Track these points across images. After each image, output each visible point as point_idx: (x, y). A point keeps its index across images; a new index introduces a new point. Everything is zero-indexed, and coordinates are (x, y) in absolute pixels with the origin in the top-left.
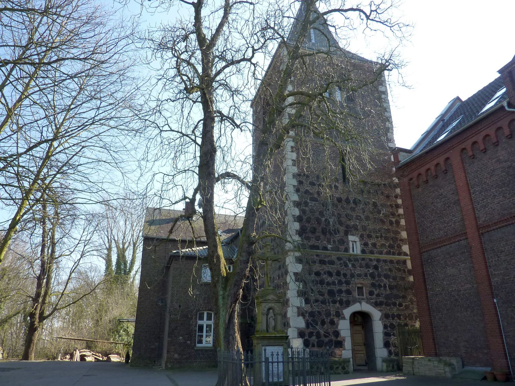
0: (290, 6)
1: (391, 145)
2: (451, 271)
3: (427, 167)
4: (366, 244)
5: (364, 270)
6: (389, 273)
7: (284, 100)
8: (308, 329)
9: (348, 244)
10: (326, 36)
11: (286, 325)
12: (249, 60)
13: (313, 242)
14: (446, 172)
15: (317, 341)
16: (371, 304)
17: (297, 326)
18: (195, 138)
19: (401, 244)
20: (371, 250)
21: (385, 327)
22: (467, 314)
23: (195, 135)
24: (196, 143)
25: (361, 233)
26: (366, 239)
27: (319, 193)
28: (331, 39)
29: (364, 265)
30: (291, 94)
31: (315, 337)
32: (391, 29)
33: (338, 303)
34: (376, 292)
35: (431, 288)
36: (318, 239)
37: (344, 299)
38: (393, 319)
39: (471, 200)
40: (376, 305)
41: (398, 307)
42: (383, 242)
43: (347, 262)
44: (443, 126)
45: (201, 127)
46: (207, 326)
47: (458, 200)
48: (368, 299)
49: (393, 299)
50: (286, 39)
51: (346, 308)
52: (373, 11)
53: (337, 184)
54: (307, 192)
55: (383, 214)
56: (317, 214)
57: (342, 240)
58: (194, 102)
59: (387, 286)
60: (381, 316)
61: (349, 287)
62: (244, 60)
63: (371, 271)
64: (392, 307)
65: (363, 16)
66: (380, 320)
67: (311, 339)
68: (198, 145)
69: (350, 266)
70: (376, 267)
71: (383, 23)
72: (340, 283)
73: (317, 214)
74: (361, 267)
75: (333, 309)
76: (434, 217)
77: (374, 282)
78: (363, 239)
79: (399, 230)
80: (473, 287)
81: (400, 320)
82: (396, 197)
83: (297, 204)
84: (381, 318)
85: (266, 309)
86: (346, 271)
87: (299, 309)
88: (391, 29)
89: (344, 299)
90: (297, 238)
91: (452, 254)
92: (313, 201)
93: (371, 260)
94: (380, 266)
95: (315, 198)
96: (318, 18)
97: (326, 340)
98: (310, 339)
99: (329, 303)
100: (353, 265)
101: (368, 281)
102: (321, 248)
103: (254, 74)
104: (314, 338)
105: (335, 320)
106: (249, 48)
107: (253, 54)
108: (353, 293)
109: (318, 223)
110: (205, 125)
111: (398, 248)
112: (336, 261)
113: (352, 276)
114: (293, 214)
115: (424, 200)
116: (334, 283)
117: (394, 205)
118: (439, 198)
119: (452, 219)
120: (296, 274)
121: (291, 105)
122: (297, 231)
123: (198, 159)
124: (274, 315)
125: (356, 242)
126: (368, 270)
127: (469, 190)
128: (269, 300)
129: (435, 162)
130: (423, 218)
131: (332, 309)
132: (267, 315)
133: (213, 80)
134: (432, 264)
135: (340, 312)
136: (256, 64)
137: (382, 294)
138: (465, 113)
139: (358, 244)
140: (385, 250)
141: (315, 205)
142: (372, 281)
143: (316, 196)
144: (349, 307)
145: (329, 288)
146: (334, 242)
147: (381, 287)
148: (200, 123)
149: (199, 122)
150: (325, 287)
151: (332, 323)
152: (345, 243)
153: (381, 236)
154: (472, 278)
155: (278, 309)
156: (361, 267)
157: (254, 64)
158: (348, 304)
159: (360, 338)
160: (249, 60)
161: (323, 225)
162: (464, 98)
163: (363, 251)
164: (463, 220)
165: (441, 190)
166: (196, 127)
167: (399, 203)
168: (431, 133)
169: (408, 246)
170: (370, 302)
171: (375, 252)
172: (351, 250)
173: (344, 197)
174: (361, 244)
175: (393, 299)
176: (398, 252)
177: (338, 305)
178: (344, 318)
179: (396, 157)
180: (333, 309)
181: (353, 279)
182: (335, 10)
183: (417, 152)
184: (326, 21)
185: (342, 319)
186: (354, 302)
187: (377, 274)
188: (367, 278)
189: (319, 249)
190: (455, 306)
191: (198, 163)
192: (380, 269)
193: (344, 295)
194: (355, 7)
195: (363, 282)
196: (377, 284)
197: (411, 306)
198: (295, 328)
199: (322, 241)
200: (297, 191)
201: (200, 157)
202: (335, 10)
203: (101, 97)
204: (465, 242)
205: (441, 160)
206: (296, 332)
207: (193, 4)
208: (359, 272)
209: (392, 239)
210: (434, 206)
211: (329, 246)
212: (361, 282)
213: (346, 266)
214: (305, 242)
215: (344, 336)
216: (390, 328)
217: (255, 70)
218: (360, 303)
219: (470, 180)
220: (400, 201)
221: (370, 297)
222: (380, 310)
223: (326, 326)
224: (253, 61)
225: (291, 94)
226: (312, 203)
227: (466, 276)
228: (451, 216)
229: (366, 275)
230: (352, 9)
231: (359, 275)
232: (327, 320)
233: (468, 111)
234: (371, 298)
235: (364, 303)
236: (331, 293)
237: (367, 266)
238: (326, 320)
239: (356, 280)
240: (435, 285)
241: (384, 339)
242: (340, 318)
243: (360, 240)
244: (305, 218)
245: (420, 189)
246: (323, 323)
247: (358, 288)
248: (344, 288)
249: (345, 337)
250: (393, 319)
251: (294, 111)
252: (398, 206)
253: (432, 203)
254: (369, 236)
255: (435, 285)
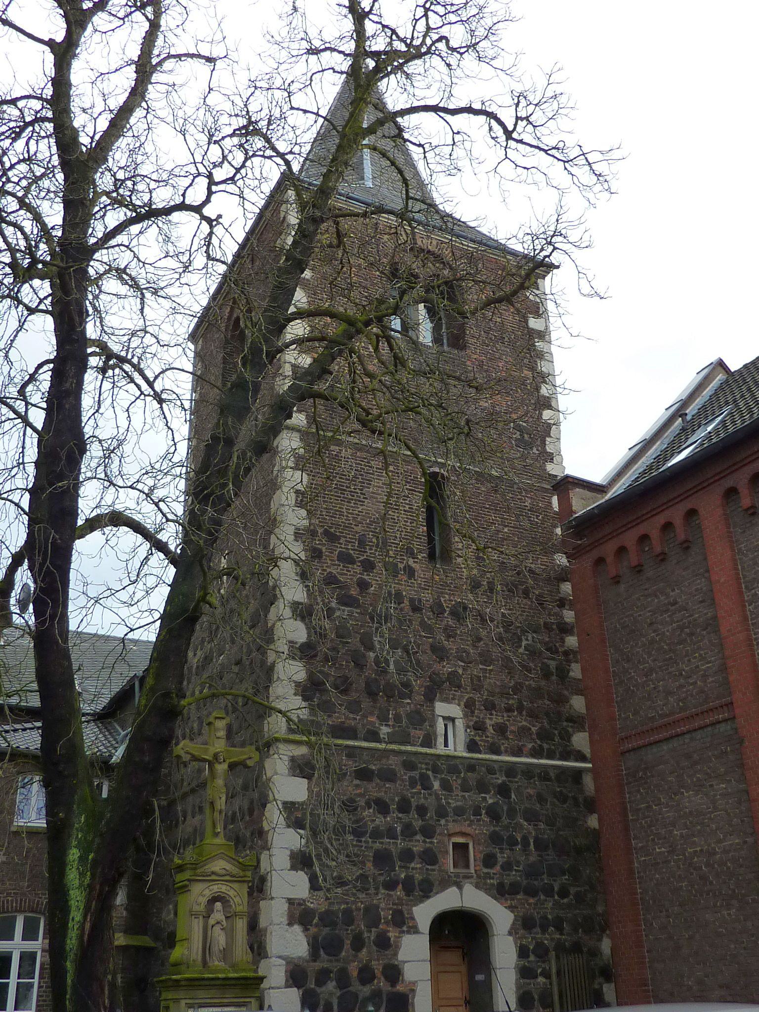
0: (311, 80)
1: (551, 468)
2: (692, 800)
3: (642, 529)
4: (479, 727)
5: (474, 798)
6: (538, 807)
7: (281, 328)
8: (315, 961)
9: (433, 725)
10: (400, 172)
11: (258, 949)
12: (197, 209)
13: (341, 716)
14: (686, 546)
15: (338, 994)
16: (488, 890)
17: (285, 953)
18: (27, 410)
19: (570, 730)
20: (493, 744)
21: (523, 952)
22: (729, 914)
23: (25, 399)
24: (27, 423)
25: (467, 696)
26: (480, 713)
27: (363, 585)
28: (412, 183)
29: (472, 783)
30: (300, 315)
31: (334, 983)
32: (566, 169)
33: (400, 887)
34: (501, 859)
35: (642, 847)
36: (354, 706)
37: (418, 877)
38: (544, 929)
39: (746, 619)
40: (501, 892)
41: (556, 897)
42: (524, 723)
43: (430, 773)
44: (683, 429)
45: (45, 378)
46: (23, 956)
47: (715, 618)
48: (479, 877)
49: (545, 876)
50: (296, 167)
51: (421, 902)
52: (522, 119)
53: (411, 561)
54: (330, 580)
55: (526, 649)
56: (354, 642)
57: (418, 712)
58: (32, 311)
59: (532, 841)
60: (514, 924)
61: (431, 843)
62: (182, 207)
63: (490, 801)
64: (542, 897)
65: (498, 131)
66: (510, 934)
67: (323, 989)
68: (34, 429)
69: (436, 785)
70: (503, 791)
71: (545, 151)
72: (408, 831)
73: (354, 642)
74: (465, 788)
75: (384, 902)
76: (655, 660)
77: (497, 829)
78: (473, 712)
79: (566, 692)
80: (745, 842)
81: (561, 934)
82: (562, 603)
83: (302, 612)
84: (512, 928)
85: (203, 900)
86: (425, 798)
87: (293, 904)
88: (566, 169)
89: (418, 877)
90: (297, 702)
91: (696, 757)
92: (346, 605)
93: (491, 771)
94: (513, 786)
95: (351, 596)
96: (380, 123)
97: (366, 991)
98: (319, 990)
99: (377, 889)
100: (446, 786)
101: (483, 827)
102: (362, 733)
103: (208, 244)
104: (331, 985)
105: (390, 934)
106: (200, 178)
107: (210, 193)
108: (441, 860)
109: (357, 665)
110: (58, 376)
111: (562, 738)
112: (401, 771)
113: (442, 813)
114: (290, 636)
115: (632, 615)
116: (391, 833)
117: (554, 627)
118: (667, 611)
119: (697, 667)
120: (289, 807)
121: (299, 341)
122: (298, 684)
123: (31, 469)
124: (227, 918)
125: (453, 720)
126: (485, 799)
127: (741, 593)
128: (213, 873)
129: (661, 519)
130: (628, 661)
131: (382, 905)
132: (207, 917)
133: (89, 252)
134: (646, 783)
135: (405, 912)
136: (216, 220)
137: (518, 863)
138: (735, 401)
139: (459, 723)
140: (530, 746)
141: (350, 615)
142: (492, 828)
143: (354, 592)
144: (428, 897)
145: (377, 846)
146: (397, 718)
147: (516, 843)
148: (45, 368)
149: (40, 366)
150: (366, 842)
151: (384, 944)
152: (427, 723)
153: (520, 708)
154: (742, 821)
155: (237, 900)
156: (464, 790)
157: (209, 221)
158: (426, 890)
159: (456, 987)
160: (197, 209)
161: (370, 672)
162: (734, 365)
163: (472, 746)
164: (724, 669)
165: (673, 590)
166: (32, 378)
167: (567, 620)
168: (654, 444)
169: (587, 734)
170: (485, 884)
171: (502, 748)
172: (441, 740)
173: (427, 597)
174: (468, 727)
175: (545, 876)
176: (560, 749)
177: (399, 892)
178: (414, 930)
179: (565, 502)
180: (384, 902)
181: (443, 822)
182: (426, 108)
183: (618, 489)
184: (400, 130)
185: (408, 932)
186: (445, 883)
187: (505, 808)
188: (479, 820)
189: (355, 737)
190: (701, 895)
191: (31, 479)
192: (513, 796)
193: (416, 864)
194: (477, 106)
195: (468, 830)
196: (505, 835)
197: (589, 896)
198: (280, 957)
199: (365, 716)
200: (303, 576)
201: (37, 464)
202: (426, 108)
203: (134, 136)
204: (729, 727)
205: (676, 515)
206: (283, 969)
207: (51, 43)
208: (459, 803)
209: (547, 714)
210: (654, 631)
211: (384, 730)
212: (464, 831)
213: (426, 785)
214: (321, 717)
215: (412, 979)
216: (536, 956)
217: (211, 234)
218: (460, 888)
219: (743, 568)
220: (569, 616)
221: (486, 870)
222: (511, 908)
223: (365, 950)
224: (207, 211)
225: (300, 315)
226: (344, 611)
227: (728, 814)
228: (695, 658)
229: (477, 812)
230: (469, 110)
231: (459, 812)
232: (371, 936)
233: (742, 396)
234: (488, 873)
235: (468, 888)
236: (382, 859)
237: (482, 787)
238: (366, 935)
239: (451, 825)
240: (653, 840)
241: (518, 987)
242: (405, 928)
243: (466, 716)
244: (323, 649)
245: (622, 587)
246: (358, 943)
247: (455, 845)
248: (418, 845)
249: (414, 983)
250: (544, 929)
251: (306, 361)
252: (565, 629)
253: (651, 624)
254: (490, 707)
255: (653, 840)
